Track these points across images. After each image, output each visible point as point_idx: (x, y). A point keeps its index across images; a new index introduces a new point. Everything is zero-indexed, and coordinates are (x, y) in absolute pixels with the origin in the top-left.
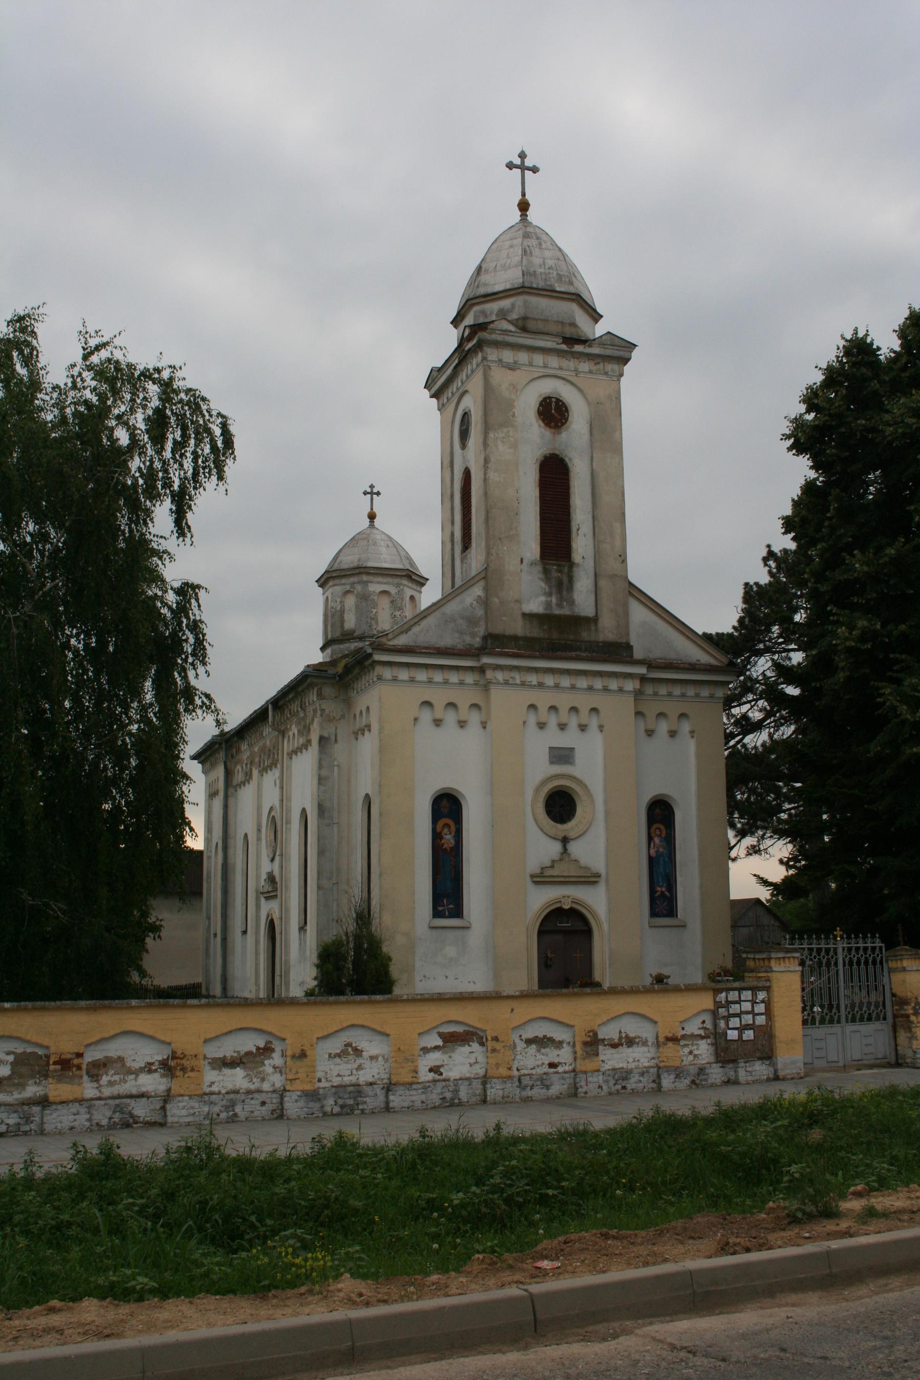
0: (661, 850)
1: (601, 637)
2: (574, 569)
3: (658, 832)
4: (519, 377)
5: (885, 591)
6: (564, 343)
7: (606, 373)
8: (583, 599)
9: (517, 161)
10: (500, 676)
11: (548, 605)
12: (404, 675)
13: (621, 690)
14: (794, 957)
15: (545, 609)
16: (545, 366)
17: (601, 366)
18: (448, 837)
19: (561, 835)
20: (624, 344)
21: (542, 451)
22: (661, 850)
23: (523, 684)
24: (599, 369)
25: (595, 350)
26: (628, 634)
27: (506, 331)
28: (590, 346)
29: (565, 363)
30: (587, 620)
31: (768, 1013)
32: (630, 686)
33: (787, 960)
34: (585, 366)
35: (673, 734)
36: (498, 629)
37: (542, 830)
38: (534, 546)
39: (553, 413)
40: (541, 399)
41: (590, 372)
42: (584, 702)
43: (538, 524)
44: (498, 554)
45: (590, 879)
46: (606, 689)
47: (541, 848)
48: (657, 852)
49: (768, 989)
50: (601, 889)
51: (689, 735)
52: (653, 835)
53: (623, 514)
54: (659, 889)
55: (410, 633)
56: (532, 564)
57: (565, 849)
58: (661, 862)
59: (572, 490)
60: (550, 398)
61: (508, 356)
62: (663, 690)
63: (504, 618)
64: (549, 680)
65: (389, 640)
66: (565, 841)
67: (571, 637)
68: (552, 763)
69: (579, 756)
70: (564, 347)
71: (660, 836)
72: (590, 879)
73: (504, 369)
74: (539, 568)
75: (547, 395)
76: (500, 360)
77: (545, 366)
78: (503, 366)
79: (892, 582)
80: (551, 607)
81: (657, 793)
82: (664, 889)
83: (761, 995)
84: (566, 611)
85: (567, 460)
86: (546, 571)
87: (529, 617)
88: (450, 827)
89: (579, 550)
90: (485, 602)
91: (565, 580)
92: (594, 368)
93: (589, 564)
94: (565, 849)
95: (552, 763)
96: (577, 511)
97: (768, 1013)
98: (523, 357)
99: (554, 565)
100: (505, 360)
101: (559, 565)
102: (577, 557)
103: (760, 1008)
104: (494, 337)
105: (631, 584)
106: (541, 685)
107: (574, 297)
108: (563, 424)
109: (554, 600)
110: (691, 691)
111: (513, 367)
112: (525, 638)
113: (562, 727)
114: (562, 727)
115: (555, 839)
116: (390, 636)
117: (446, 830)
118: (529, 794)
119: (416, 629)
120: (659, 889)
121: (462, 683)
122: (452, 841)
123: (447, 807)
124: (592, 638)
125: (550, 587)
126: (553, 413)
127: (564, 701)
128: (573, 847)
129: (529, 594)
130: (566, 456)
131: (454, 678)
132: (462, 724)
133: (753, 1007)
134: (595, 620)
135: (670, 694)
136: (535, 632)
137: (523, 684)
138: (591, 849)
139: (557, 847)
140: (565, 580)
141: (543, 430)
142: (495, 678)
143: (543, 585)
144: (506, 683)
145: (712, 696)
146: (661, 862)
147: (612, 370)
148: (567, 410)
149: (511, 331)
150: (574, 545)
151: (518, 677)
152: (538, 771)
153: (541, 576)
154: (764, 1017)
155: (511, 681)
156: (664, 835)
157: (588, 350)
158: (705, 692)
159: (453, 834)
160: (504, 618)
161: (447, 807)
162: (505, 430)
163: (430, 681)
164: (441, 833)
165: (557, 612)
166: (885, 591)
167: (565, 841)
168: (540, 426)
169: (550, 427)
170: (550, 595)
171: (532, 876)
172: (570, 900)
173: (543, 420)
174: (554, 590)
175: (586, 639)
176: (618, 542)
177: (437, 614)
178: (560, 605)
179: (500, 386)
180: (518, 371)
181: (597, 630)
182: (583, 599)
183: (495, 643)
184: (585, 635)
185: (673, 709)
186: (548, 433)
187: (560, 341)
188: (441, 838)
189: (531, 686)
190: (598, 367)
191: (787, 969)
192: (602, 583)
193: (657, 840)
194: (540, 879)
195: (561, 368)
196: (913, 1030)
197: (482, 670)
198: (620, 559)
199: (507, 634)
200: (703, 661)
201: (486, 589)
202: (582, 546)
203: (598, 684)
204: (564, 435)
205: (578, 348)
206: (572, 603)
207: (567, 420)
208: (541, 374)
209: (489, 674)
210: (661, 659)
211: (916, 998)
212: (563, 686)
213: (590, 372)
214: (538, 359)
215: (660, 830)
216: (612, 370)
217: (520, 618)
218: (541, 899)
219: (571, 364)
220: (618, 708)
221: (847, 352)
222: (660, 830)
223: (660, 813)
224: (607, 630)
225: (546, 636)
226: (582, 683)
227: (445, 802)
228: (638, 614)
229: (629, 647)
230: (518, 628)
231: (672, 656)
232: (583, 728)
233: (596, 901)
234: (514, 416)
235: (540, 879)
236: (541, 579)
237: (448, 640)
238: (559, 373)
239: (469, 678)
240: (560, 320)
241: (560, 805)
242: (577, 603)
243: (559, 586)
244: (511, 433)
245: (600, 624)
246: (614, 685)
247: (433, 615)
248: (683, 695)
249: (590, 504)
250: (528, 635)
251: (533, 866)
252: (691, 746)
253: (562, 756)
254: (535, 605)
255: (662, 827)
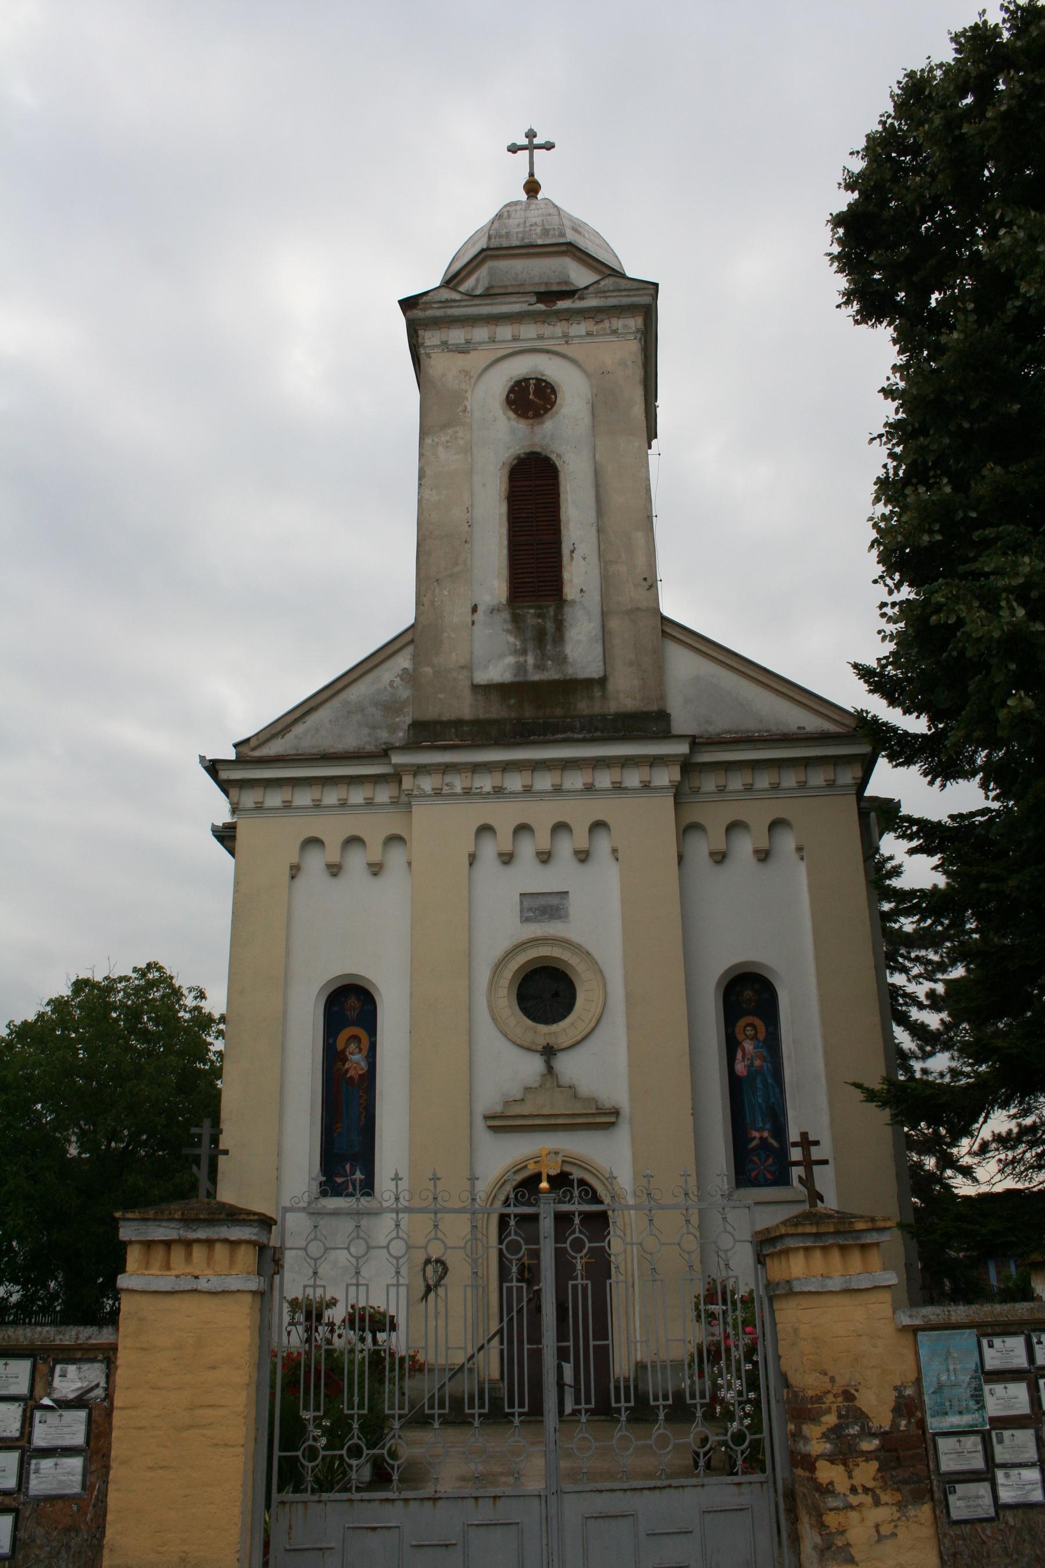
0: (757, 1062)
1: (613, 707)
2: (567, 609)
3: (750, 1032)
4: (476, 360)
5: (966, 425)
6: (539, 301)
7: (614, 332)
8: (582, 649)
9: (525, 142)
10: (427, 784)
11: (521, 668)
12: (274, 799)
13: (646, 786)
14: (234, 1244)
15: (516, 675)
16: (515, 339)
17: (606, 324)
18: (356, 1057)
19: (542, 1042)
20: (636, 285)
21: (511, 451)
22: (757, 1062)
23: (467, 792)
24: (604, 329)
25: (591, 302)
26: (662, 697)
27: (447, 301)
28: (582, 298)
29: (547, 330)
30: (588, 683)
31: (96, 1449)
32: (664, 777)
33: (220, 1251)
34: (579, 329)
35: (763, 856)
36: (431, 713)
37: (505, 1035)
38: (496, 583)
39: (531, 399)
40: (512, 383)
41: (589, 334)
42: (580, 813)
43: (505, 551)
44: (432, 603)
45: (602, 1119)
46: (618, 788)
47: (506, 1067)
48: (749, 1067)
49: (108, 1356)
50: (622, 1136)
51: (795, 857)
52: (740, 1037)
53: (649, 518)
54: (755, 1134)
55: (287, 736)
56: (493, 611)
57: (550, 1069)
58: (760, 1085)
59: (562, 496)
60: (527, 380)
61: (456, 336)
62: (736, 782)
63: (441, 696)
64: (514, 782)
65: (254, 749)
66: (549, 1052)
67: (559, 712)
68: (525, 920)
69: (574, 905)
70: (541, 307)
71: (754, 1037)
72: (602, 1119)
73: (451, 354)
74: (506, 615)
75: (521, 377)
76: (445, 343)
77: (515, 339)
78: (450, 351)
79: (975, 405)
80: (526, 671)
81: (743, 959)
82: (766, 1134)
83: (70, 1381)
84: (552, 674)
85: (553, 457)
86: (516, 620)
87: (483, 690)
88: (360, 1041)
89: (575, 581)
90: (410, 677)
91: (550, 626)
92: (594, 329)
93: (593, 600)
94: (550, 1069)
95: (525, 920)
96: (572, 525)
97: (96, 1449)
98: (480, 333)
99: (530, 607)
100: (451, 342)
101: (539, 607)
102: (570, 592)
103: (72, 1429)
104: (430, 313)
105: (665, 620)
106: (498, 791)
107: (564, 248)
108: (547, 411)
109: (530, 660)
110: (789, 779)
111: (464, 349)
112: (476, 723)
113: (545, 857)
114: (545, 857)
115: (529, 1049)
116: (253, 743)
117: (353, 1046)
118: (483, 975)
119: (299, 729)
120: (755, 1134)
121: (369, 803)
122: (363, 1064)
123: (350, 1007)
124: (597, 709)
125: (524, 641)
126: (531, 399)
127: (542, 815)
128: (568, 1065)
129: (494, 656)
130: (552, 452)
131: (357, 796)
132: (376, 869)
133: (27, 1422)
134: (602, 682)
135: (749, 788)
136: (496, 711)
137: (467, 792)
138: (601, 1061)
139: (535, 1065)
140: (550, 626)
141: (514, 423)
142: (419, 788)
143: (511, 639)
144: (438, 793)
145: (831, 784)
146: (760, 1085)
147: (625, 326)
148: (554, 392)
149: (455, 301)
150: (566, 575)
151: (458, 783)
152: (500, 930)
153: (509, 626)
154: (76, 1463)
155: (446, 790)
156: (761, 1036)
157: (579, 304)
158: (818, 778)
159: (365, 1052)
160: (441, 696)
161: (350, 1007)
162: (450, 431)
163: (317, 805)
164: (344, 1050)
165: (536, 677)
166: (966, 425)
167: (549, 1052)
168: (509, 419)
169: (527, 418)
170: (524, 652)
171: (486, 1118)
172: (560, 1159)
173: (515, 411)
174: (530, 646)
175: (586, 712)
176: (641, 560)
177: (335, 703)
178: (540, 667)
179: (444, 375)
180: (473, 353)
181: (604, 697)
182: (582, 649)
183: (427, 733)
184: (583, 707)
185: (759, 814)
186: (522, 426)
187: (534, 299)
188: (345, 1060)
189: (483, 795)
190: (601, 326)
191: (187, 1284)
192: (614, 624)
193: (748, 1046)
194: (503, 1124)
195: (541, 337)
196: (831, 1520)
197: (395, 777)
198: (646, 585)
199: (444, 719)
200: (809, 729)
201: (415, 658)
202: (579, 574)
203: (604, 780)
204: (548, 425)
205: (562, 305)
206: (562, 660)
207: (553, 404)
208: (510, 351)
209: (407, 782)
210: (730, 732)
211: (848, 1396)
212: (541, 791)
213: (589, 334)
214: (505, 332)
215: (754, 1027)
216: (625, 326)
217: (467, 693)
218: (501, 1158)
219: (559, 329)
220: (646, 818)
221: (902, 107)
222: (754, 1027)
223: (748, 997)
224: (625, 694)
225: (513, 715)
226: (575, 781)
227: (352, 1001)
228: (683, 665)
229: (663, 717)
230: (465, 707)
231: (750, 725)
232: (583, 856)
233: (612, 1159)
234: (465, 411)
235: (503, 1124)
236: (508, 631)
237: (350, 742)
238: (539, 344)
239: (383, 795)
240: (545, 280)
241: (545, 990)
242: (571, 660)
243: (540, 638)
244: (460, 434)
245: (610, 687)
246: (633, 779)
247: (328, 705)
248: (775, 787)
249: (592, 514)
250: (482, 717)
251: (488, 1100)
252: (801, 872)
253: (545, 907)
254: (498, 670)
255: (758, 1022)
